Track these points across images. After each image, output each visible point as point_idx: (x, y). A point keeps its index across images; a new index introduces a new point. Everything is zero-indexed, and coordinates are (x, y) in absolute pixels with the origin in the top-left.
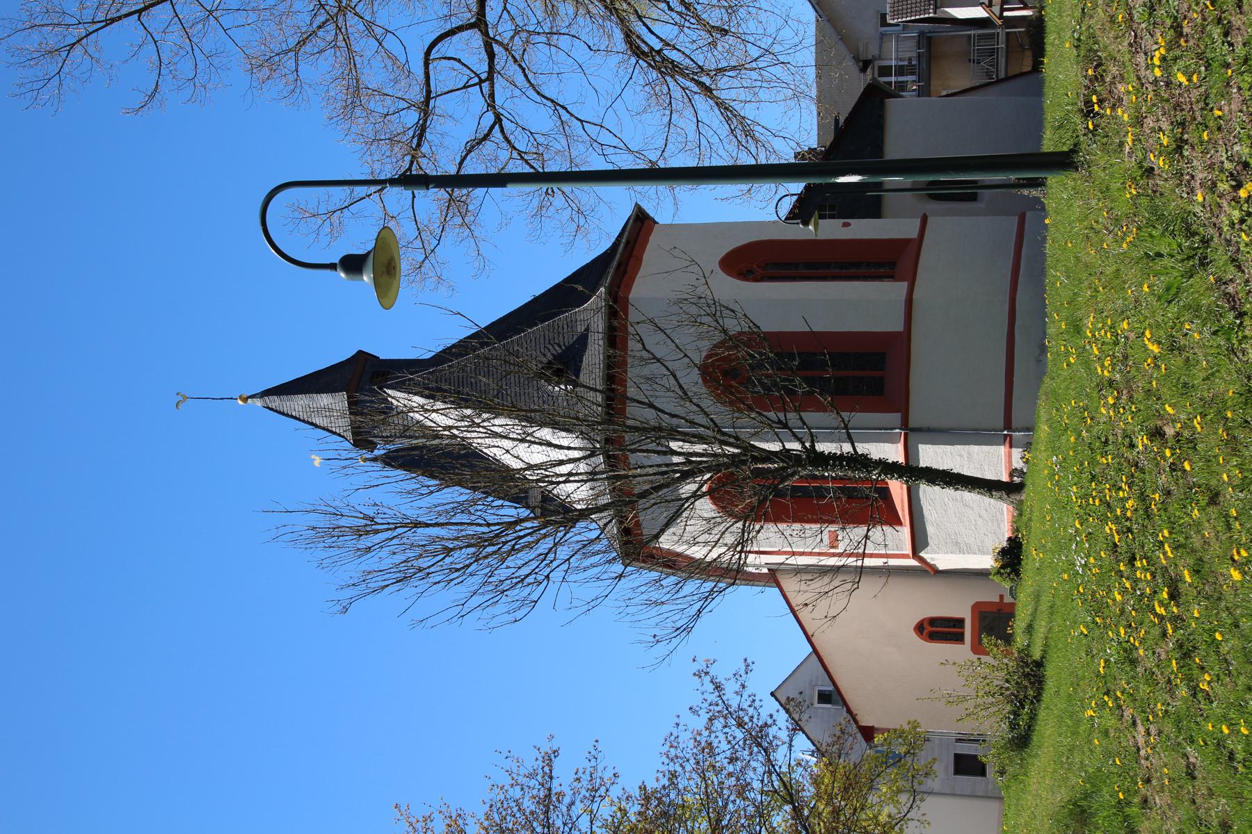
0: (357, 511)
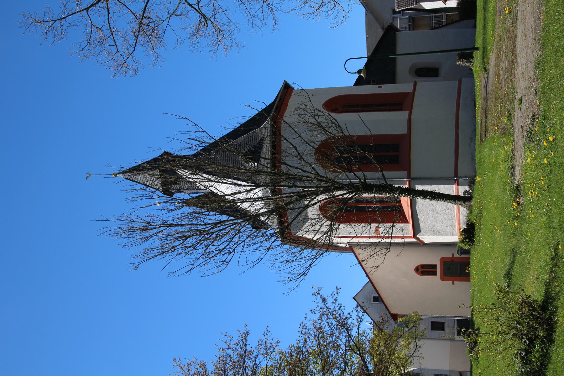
0: (141, 219)
